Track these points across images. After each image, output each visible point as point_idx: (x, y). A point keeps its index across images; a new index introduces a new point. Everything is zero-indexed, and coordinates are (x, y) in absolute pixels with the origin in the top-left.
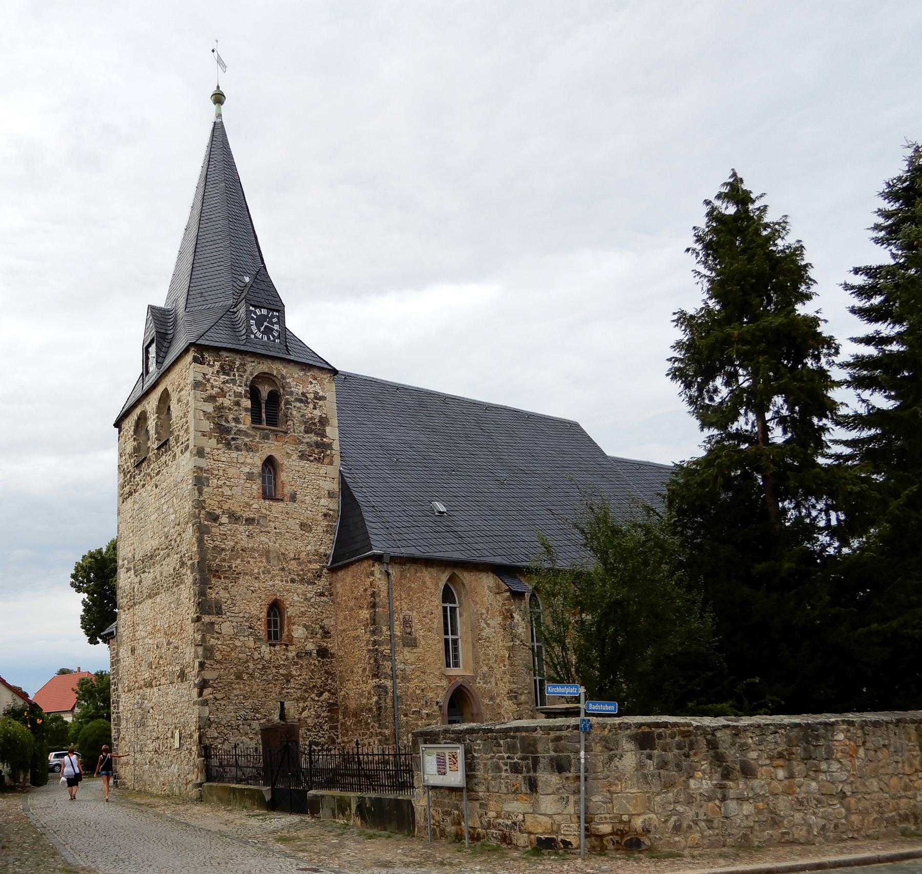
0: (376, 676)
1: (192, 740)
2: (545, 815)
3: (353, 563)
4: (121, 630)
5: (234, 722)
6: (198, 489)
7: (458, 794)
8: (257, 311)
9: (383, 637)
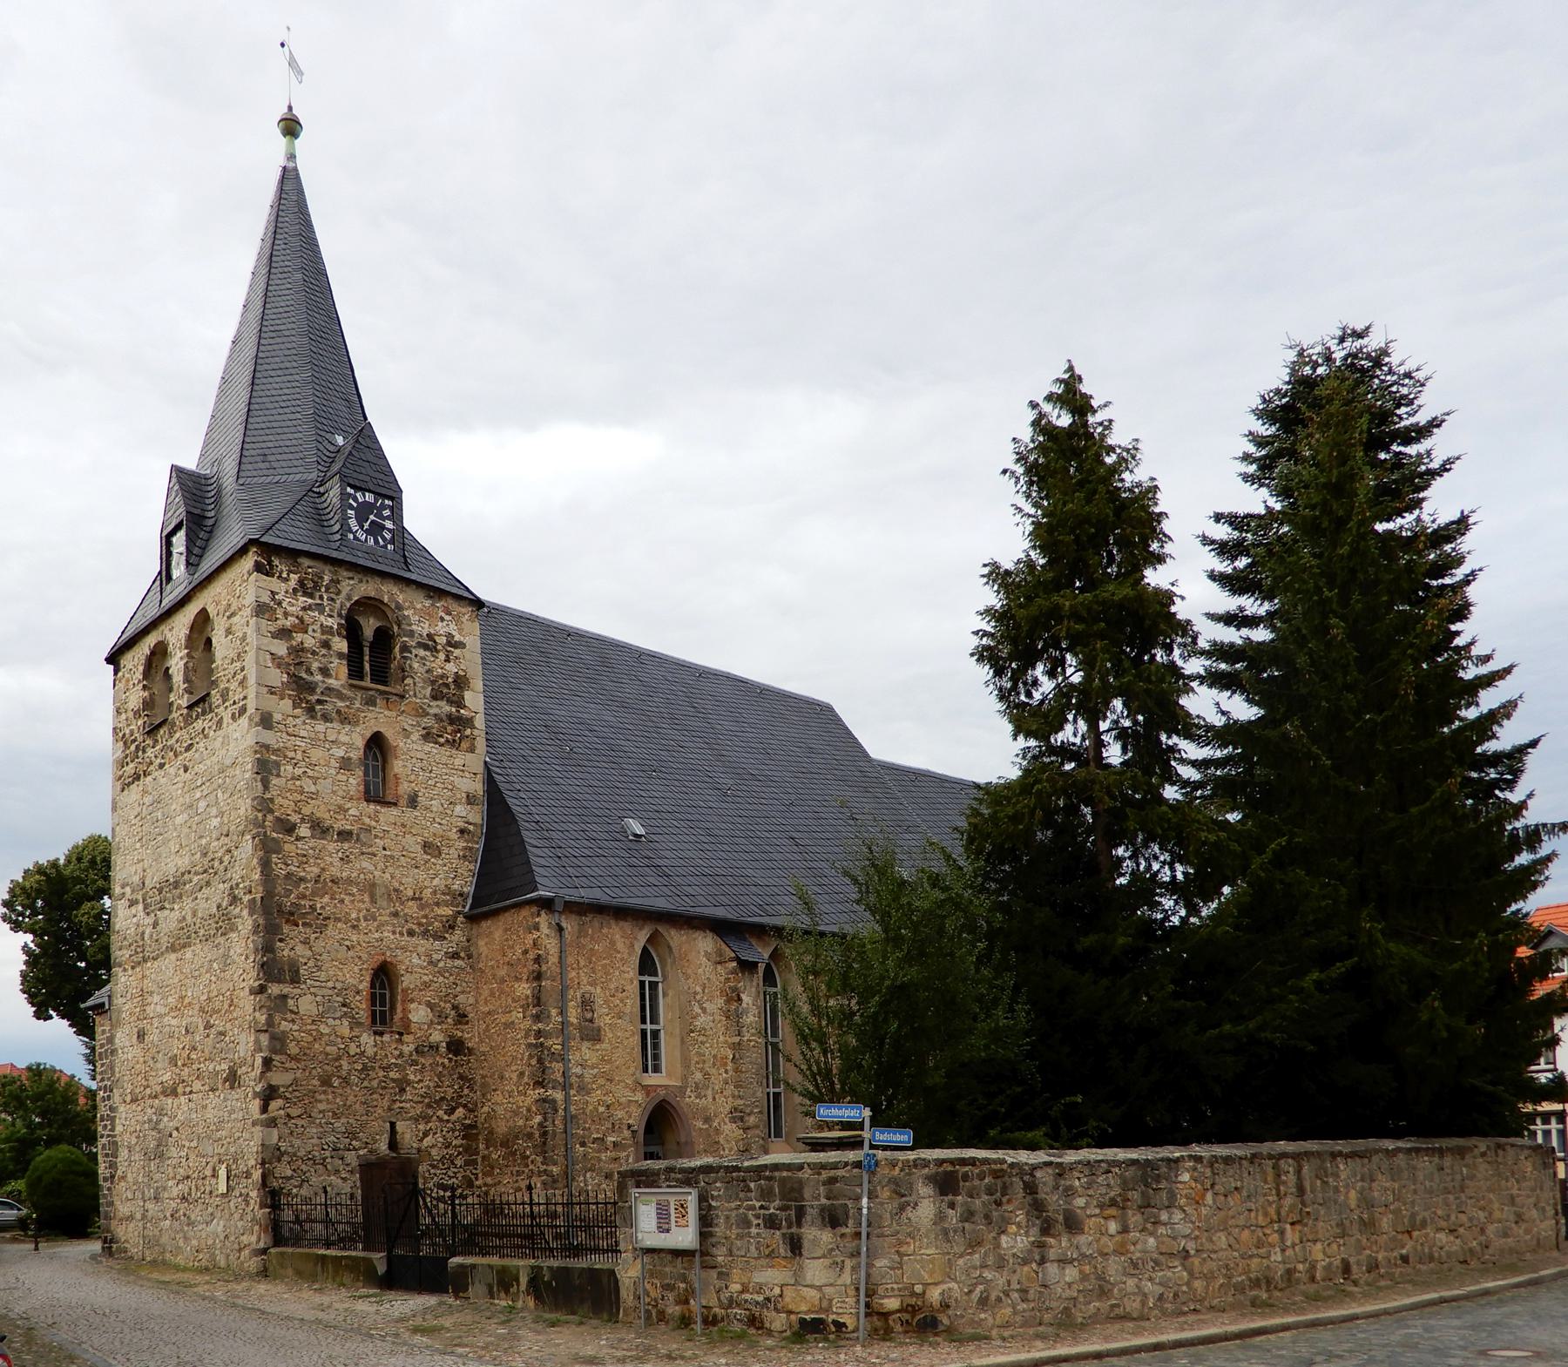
0: (540, 1084)
1: (250, 1181)
2: (811, 1286)
3: (506, 909)
4: (118, 1001)
5: (317, 1154)
6: (262, 780)
7: (685, 1259)
8: (358, 495)
9: (551, 1026)
